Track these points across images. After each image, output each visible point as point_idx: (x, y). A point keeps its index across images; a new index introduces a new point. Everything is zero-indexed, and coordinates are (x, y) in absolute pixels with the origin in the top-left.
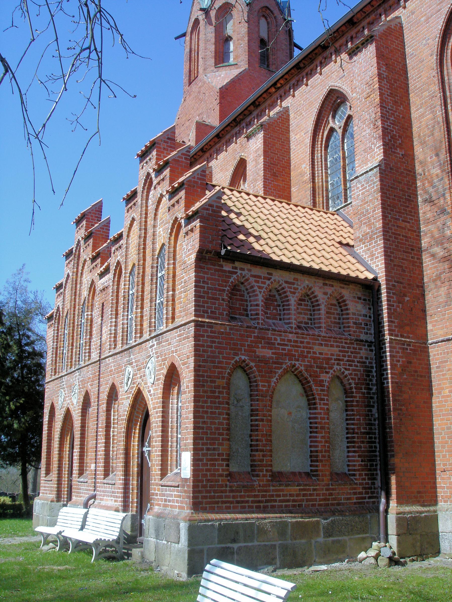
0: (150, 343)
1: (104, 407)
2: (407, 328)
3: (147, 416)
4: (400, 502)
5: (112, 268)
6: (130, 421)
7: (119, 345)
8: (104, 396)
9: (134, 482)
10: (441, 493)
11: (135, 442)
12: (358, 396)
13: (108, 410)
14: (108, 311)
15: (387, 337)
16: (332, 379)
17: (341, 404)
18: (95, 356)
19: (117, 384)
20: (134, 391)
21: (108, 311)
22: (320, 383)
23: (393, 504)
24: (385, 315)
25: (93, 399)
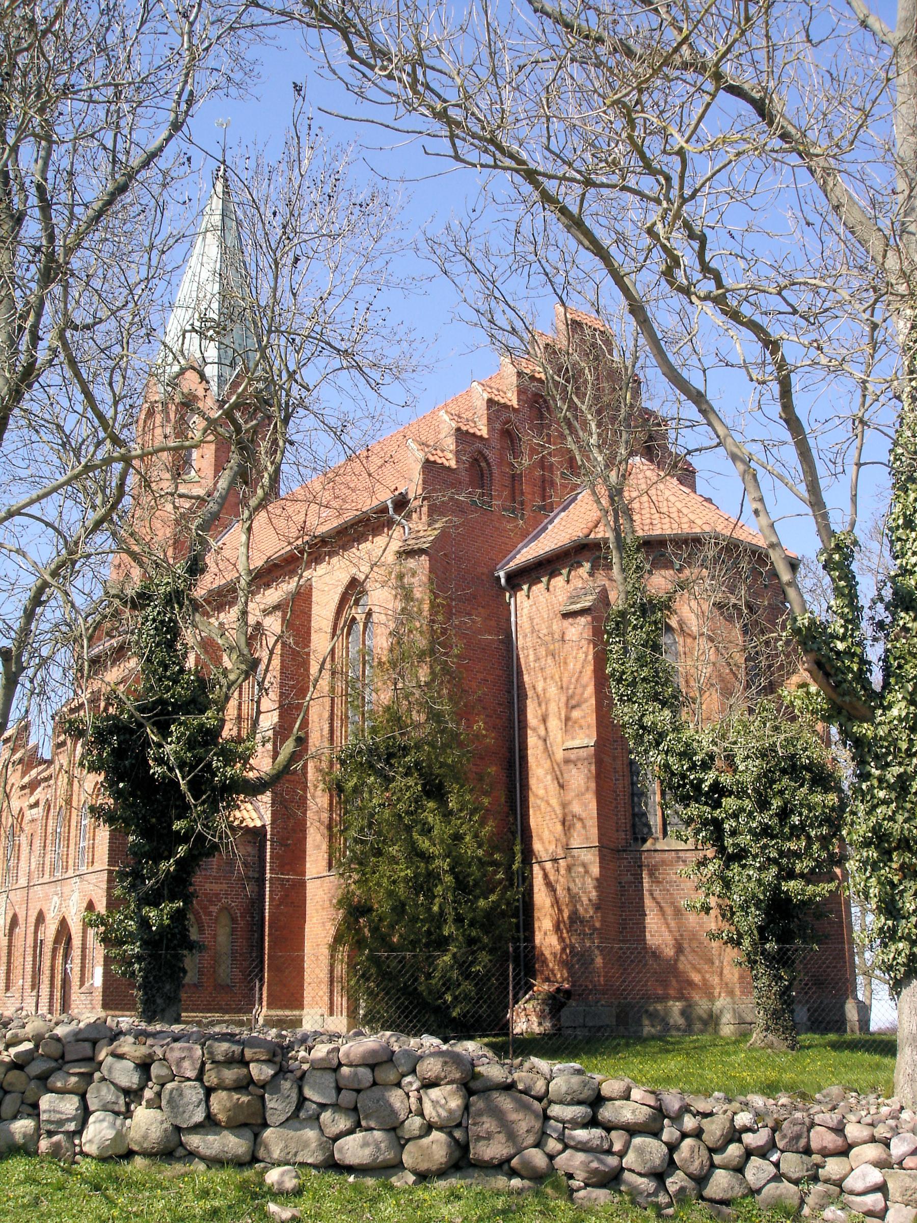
0: (74, 880)
1: (31, 929)
2: (288, 867)
3: (69, 939)
4: (270, 1006)
5: (42, 804)
6: (57, 941)
7: (47, 876)
8: (32, 920)
9: (58, 994)
10: (307, 1000)
11: (59, 960)
12: (242, 923)
13: (36, 932)
14: (37, 843)
15: (268, 876)
16: (221, 910)
17: (228, 930)
18: (23, 882)
19: (45, 911)
20: (59, 918)
21: (37, 843)
22: (210, 914)
23: (264, 1009)
24: (268, 857)
25: (21, 920)
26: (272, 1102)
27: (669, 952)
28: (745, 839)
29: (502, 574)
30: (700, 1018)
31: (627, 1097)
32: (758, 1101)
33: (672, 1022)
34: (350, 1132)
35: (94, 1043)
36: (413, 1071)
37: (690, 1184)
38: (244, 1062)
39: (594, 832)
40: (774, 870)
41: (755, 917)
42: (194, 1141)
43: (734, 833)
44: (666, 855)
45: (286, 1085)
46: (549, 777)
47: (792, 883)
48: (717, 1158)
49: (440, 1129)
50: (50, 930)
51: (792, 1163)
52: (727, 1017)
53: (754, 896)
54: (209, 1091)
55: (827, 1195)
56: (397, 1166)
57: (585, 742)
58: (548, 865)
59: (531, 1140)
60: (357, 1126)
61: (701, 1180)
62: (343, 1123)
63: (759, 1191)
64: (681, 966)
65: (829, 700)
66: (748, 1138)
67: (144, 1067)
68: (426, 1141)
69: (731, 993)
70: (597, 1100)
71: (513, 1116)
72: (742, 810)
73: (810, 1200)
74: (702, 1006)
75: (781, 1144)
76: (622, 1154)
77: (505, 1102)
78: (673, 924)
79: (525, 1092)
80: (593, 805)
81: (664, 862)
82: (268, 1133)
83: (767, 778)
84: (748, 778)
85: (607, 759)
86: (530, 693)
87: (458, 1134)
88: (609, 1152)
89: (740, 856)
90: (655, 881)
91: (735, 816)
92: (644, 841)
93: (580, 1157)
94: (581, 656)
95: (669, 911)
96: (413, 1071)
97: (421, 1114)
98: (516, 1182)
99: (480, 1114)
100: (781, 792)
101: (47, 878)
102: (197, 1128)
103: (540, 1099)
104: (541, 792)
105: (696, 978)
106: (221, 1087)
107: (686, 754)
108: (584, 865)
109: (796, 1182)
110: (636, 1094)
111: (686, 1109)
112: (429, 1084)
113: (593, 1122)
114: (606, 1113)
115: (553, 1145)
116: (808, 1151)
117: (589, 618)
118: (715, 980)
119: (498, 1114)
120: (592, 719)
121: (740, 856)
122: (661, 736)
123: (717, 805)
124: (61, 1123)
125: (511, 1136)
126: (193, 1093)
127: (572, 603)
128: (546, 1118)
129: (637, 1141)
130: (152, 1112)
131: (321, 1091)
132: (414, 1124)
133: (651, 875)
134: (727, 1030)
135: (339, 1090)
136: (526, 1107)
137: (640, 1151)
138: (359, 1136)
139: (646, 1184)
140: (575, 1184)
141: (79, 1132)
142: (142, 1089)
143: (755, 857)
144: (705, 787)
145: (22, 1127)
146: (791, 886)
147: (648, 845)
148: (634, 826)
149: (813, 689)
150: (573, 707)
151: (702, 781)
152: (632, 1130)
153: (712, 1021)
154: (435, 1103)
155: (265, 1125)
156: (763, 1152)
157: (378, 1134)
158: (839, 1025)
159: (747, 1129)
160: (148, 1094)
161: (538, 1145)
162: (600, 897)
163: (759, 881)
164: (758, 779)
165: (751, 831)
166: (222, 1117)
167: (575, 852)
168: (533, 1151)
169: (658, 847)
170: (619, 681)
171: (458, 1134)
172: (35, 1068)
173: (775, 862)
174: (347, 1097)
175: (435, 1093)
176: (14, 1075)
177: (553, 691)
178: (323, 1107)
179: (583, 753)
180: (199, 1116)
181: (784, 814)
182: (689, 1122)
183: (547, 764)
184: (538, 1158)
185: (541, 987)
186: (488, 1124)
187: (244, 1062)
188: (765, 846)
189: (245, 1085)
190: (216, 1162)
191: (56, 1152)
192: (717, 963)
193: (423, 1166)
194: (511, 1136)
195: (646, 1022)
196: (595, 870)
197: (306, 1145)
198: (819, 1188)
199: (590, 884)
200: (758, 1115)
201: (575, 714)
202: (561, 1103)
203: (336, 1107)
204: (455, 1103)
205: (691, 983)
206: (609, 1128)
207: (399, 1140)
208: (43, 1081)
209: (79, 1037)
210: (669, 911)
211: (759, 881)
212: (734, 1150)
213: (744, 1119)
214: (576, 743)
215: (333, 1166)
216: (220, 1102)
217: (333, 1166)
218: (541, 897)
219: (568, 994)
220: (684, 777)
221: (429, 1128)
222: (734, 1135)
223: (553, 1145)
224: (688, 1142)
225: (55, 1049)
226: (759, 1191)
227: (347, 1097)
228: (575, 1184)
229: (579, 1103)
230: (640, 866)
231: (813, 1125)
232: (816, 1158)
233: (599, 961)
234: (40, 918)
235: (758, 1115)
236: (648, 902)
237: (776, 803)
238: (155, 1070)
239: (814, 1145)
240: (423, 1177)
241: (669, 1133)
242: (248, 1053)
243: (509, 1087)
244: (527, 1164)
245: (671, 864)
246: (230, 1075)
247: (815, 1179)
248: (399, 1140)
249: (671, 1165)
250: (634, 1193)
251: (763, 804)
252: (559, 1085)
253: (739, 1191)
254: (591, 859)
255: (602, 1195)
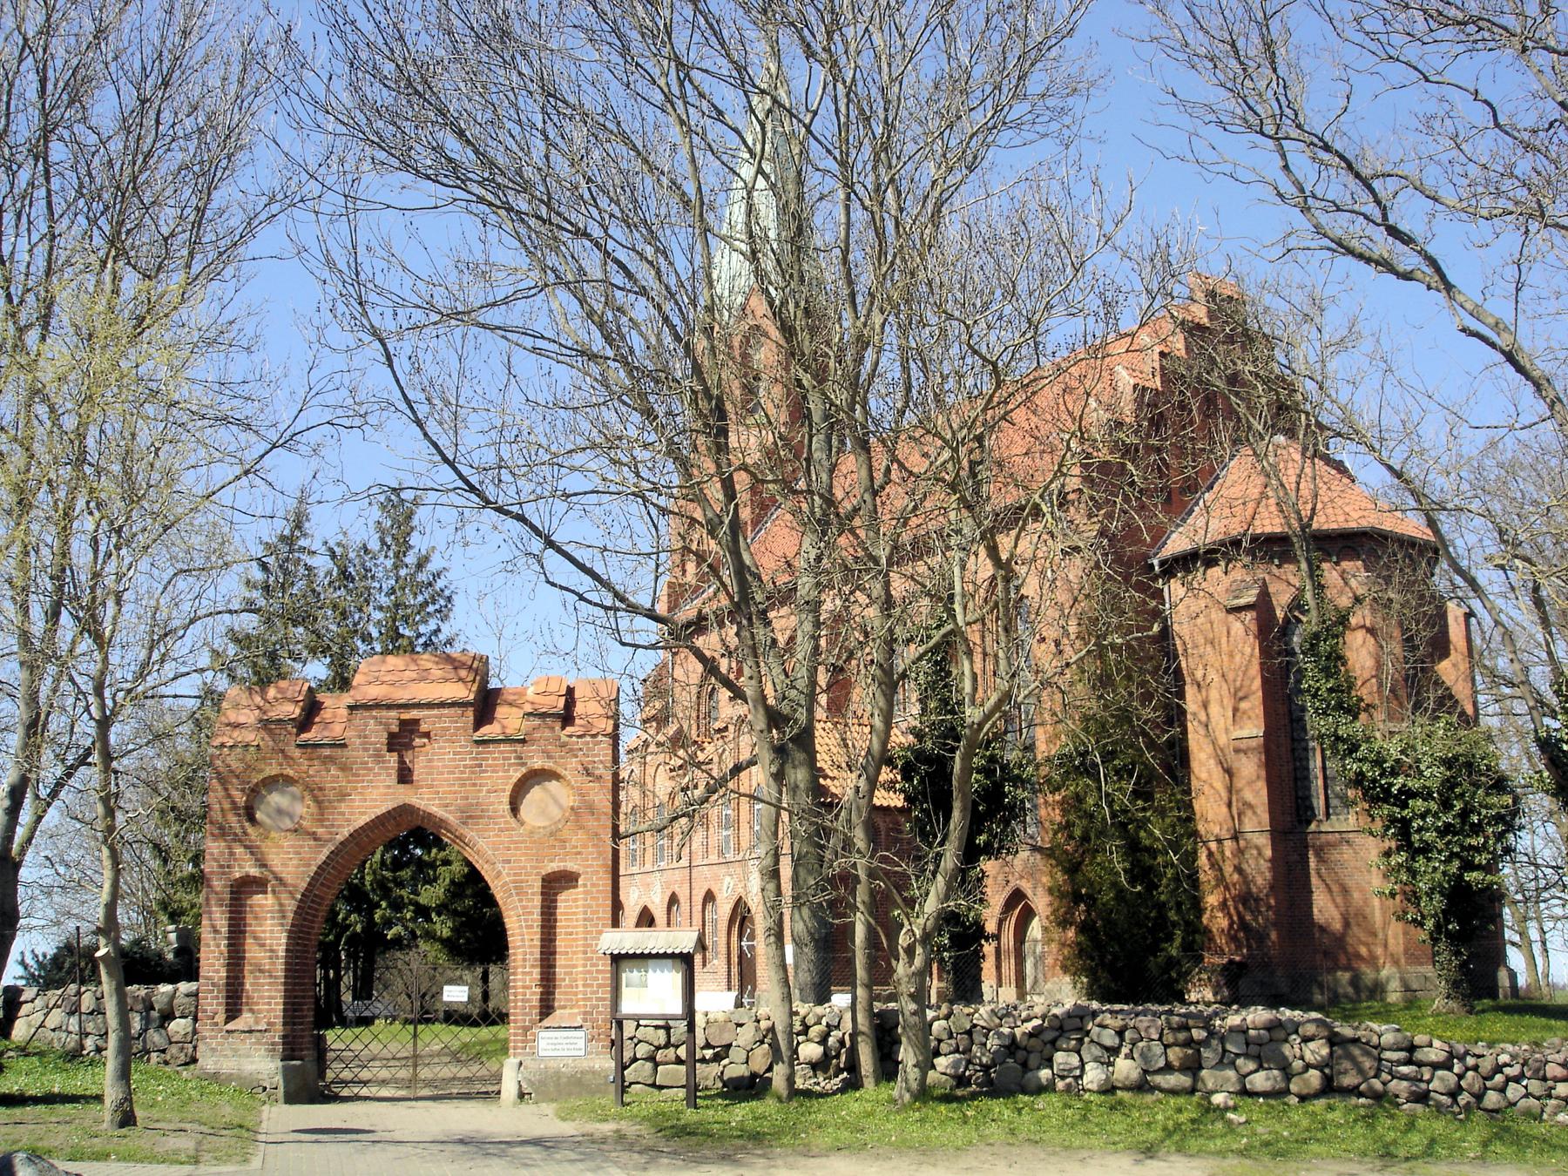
11: (734, 938)
19: (715, 890)
20: (735, 898)
23: (935, 982)
26: (1206, 1053)
27: (1337, 926)
28: (1429, 836)
29: (1156, 562)
30: (1367, 987)
31: (1431, 1045)
32: (1509, 1047)
33: (1341, 991)
34: (1256, 1071)
35: (1082, 1018)
36: (1296, 1032)
37: (1472, 1100)
38: (1187, 1028)
39: (1265, 817)
40: (1456, 863)
41: (1438, 902)
42: (1158, 1079)
43: (1420, 829)
44: (1330, 836)
45: (1214, 1042)
46: (1212, 762)
47: (1475, 874)
48: (1488, 1084)
49: (1315, 1067)
50: (724, 908)
51: (1535, 1086)
52: (1394, 985)
53: (1440, 885)
54: (1166, 1047)
55: (1558, 1106)
56: (1287, 1092)
57: (1255, 732)
58: (1213, 846)
59: (1372, 1073)
60: (1260, 1067)
61: (1479, 1097)
62: (1251, 1066)
63: (1515, 1104)
64: (1350, 940)
65: (1557, 783)
66: (1507, 1070)
67: (1120, 1033)
68: (1306, 1075)
69: (1396, 962)
70: (1412, 1048)
71: (1361, 1059)
72: (1428, 812)
73: (1548, 1110)
74: (1368, 974)
75: (1528, 1074)
76: (1428, 1082)
77: (1356, 1051)
78: (1339, 900)
79: (1367, 1043)
80: (1264, 792)
81: (1329, 844)
82: (1204, 1073)
83: (1450, 784)
84: (1434, 785)
85: (1273, 747)
86: (1188, 680)
87: (1327, 1071)
88: (1421, 1080)
89: (1426, 849)
90: (1321, 860)
91: (1423, 816)
92: (1309, 823)
93: (1405, 1084)
94: (1248, 650)
95: (1335, 888)
96: (1296, 1032)
97: (1302, 1058)
98: (1362, 1100)
99: (1340, 1057)
100: (1462, 795)
101: (713, 858)
102: (1160, 1071)
103: (1375, 1047)
104: (1204, 776)
105: (1363, 951)
106: (1175, 1044)
107: (1378, 762)
108: (1258, 848)
109: (1538, 1098)
110: (1437, 1043)
111: (1467, 1053)
112: (1307, 1040)
113: (1409, 1062)
114: (1419, 1055)
115: (1385, 1076)
116: (1544, 1079)
117: (1254, 614)
118: (1379, 951)
119: (1352, 1059)
120: (1260, 711)
121: (1426, 849)
122: (1354, 748)
123: (1404, 806)
124: (1070, 1070)
125: (1361, 1071)
126: (1157, 1048)
127: (1237, 597)
128: (1380, 1060)
129: (1440, 1073)
130: (1129, 1062)
131: (1236, 1044)
132: (1297, 1065)
133: (1317, 855)
134: (1394, 996)
135: (1247, 1044)
136: (1368, 1054)
137: (1442, 1079)
138: (1262, 1074)
139: (1445, 1100)
140: (1401, 1101)
141: (1081, 1077)
142: (1121, 1046)
143: (1440, 852)
144: (1394, 790)
145: (1045, 1074)
146: (1471, 876)
147: (1313, 827)
148: (1298, 809)
149: (1546, 774)
150: (1241, 699)
151: (1391, 785)
152: (1435, 1066)
153: (1378, 990)
154: (1313, 1052)
155: (1201, 1068)
156: (1517, 1080)
157: (1276, 1072)
158: (1492, 991)
159: (1506, 1065)
160: (1125, 1050)
161: (1376, 1076)
162: (1274, 878)
163: (1444, 873)
164: (1442, 784)
165: (1437, 829)
166: (1176, 1064)
167: (1249, 836)
168: (1374, 1081)
169: (1323, 829)
170: (1315, 696)
171: (1327, 1071)
172: (1049, 1036)
173: (1457, 855)
174: (1253, 1049)
175: (1312, 1045)
176: (1033, 1040)
177: (1213, 675)
178: (1238, 1055)
179: (1254, 743)
180: (1161, 1063)
181: (1464, 814)
182: (1470, 1061)
183: (1209, 749)
184: (1377, 1084)
185: (1211, 960)
186: (1346, 1064)
187: (1187, 1028)
188: (1449, 842)
189: (1189, 1042)
190: (1173, 1092)
191: (1068, 1088)
192: (1381, 935)
193: (1305, 1091)
194: (1361, 1071)
195: (1316, 990)
196: (1268, 853)
197: (1228, 1080)
198: (1553, 1102)
199: (1265, 865)
200: (1513, 1057)
201: (1243, 705)
202: (1390, 1049)
203: (1247, 1056)
204: (1325, 1051)
205: (1358, 956)
206: (1420, 1064)
207: (1288, 1074)
208: (1054, 1045)
209: (1069, 1015)
210: (1335, 888)
211: (1444, 873)
212: (1499, 1078)
213: (1504, 1058)
214: (1245, 733)
215: (1245, 1092)
216: (1175, 1055)
217: (1245, 1092)
218: (1206, 875)
219: (1241, 966)
220: (1374, 781)
221: (1308, 1066)
222: (1498, 1069)
223: (1385, 1076)
224: (1470, 1074)
225: (1056, 1023)
226: (1515, 1104)
227: (1253, 1049)
228: (1401, 1101)
229: (1401, 1050)
230: (1306, 847)
231: (1547, 1062)
232: (1550, 1083)
233: (1274, 936)
234: (709, 897)
235: (1513, 1057)
236: (1314, 880)
237: (1458, 805)
238: (1128, 1035)
239: (1549, 1075)
240: (1303, 1098)
241: (1457, 1068)
242: (1191, 1022)
243: (1356, 1041)
244: (1371, 1088)
245: (1333, 845)
246: (1182, 1036)
247: (1550, 1096)
248: (1288, 1074)
249: (1460, 1089)
250: (1439, 1106)
251: (1446, 805)
252: (1389, 1038)
253: (1503, 1104)
254: (1264, 841)
255: (1419, 1108)
